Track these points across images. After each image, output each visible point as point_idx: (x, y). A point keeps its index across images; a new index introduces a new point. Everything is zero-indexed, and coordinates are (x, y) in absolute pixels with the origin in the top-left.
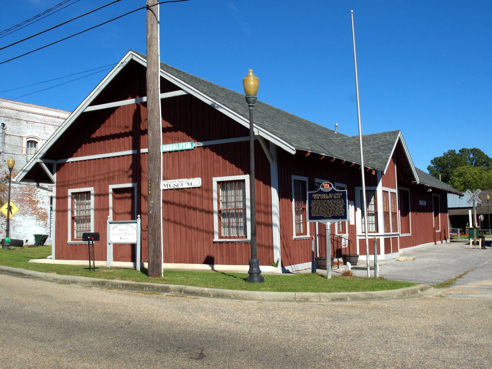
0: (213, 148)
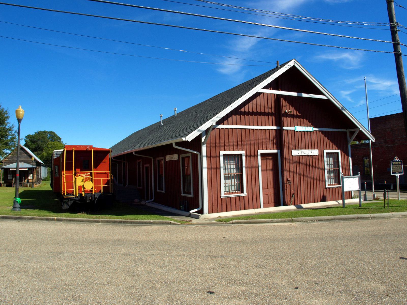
0: (323, 132)
